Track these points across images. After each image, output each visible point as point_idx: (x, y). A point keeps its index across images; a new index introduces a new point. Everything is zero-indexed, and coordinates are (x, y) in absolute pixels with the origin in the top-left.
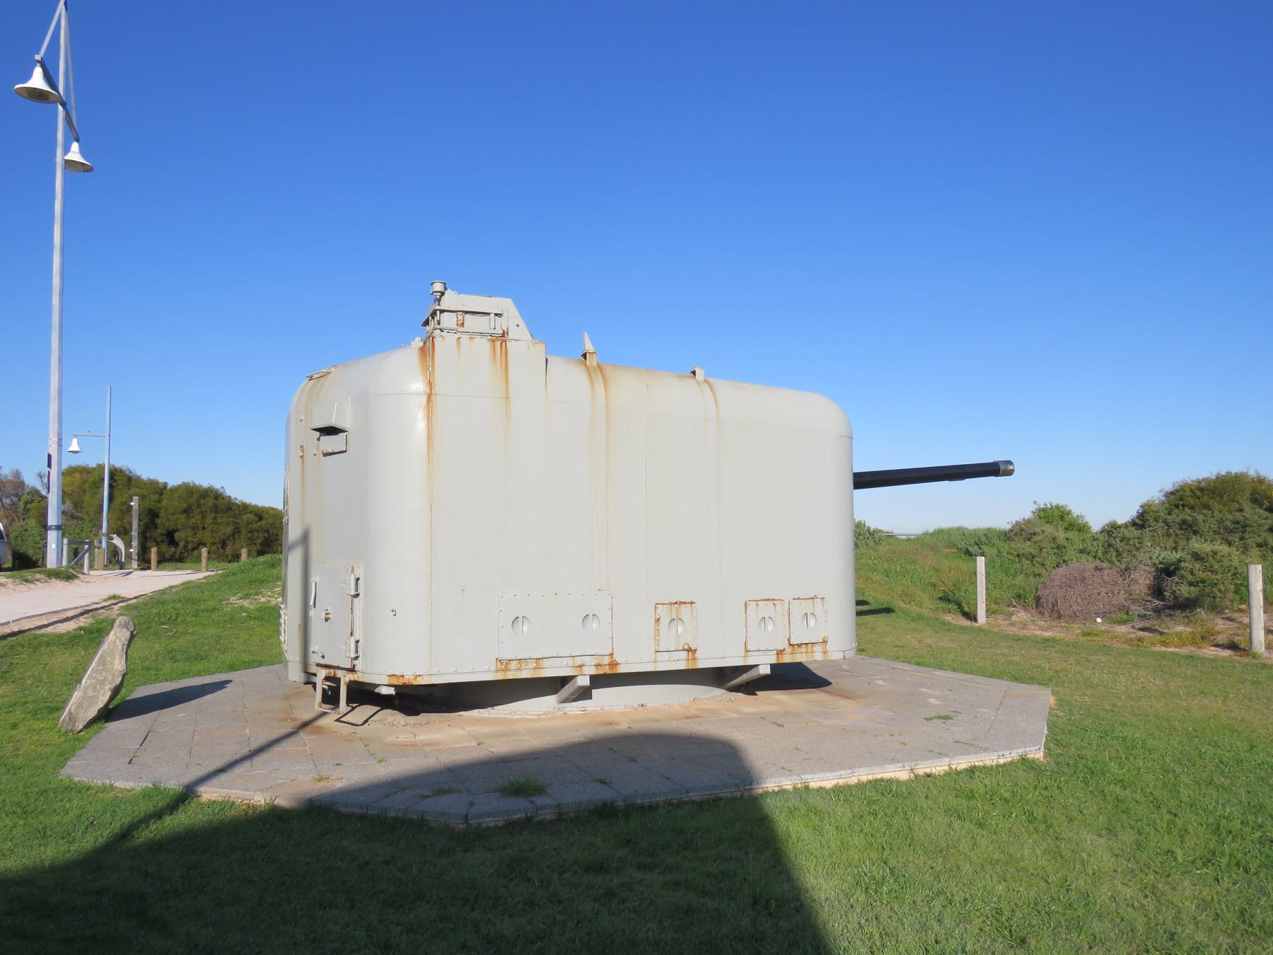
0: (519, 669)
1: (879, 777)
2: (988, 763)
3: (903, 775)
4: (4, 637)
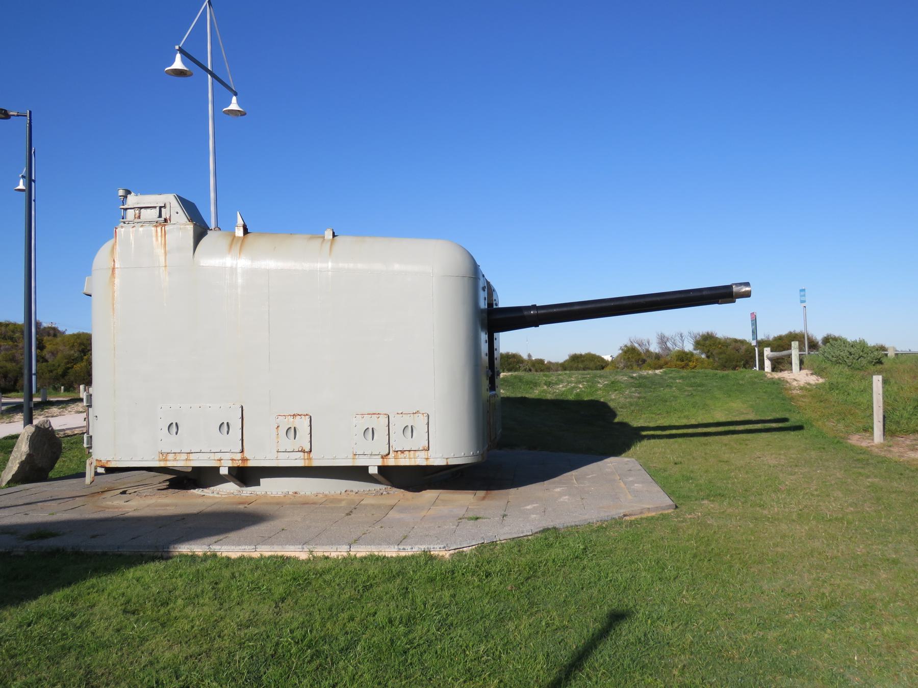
0: (175, 460)
1: (280, 554)
2: (388, 555)
3: (303, 556)
4: (915, 432)
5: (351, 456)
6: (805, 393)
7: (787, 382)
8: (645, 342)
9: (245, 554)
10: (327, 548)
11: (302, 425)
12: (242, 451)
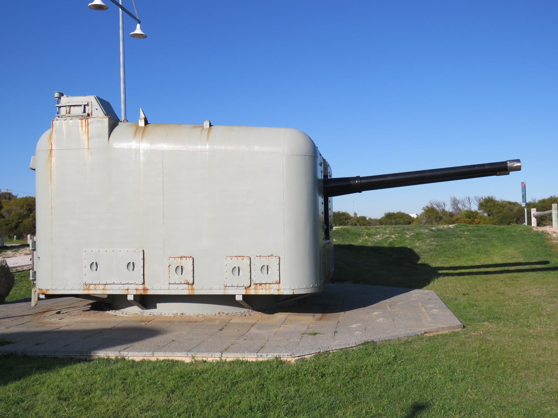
0: (95, 289)
1: (171, 358)
2: (250, 360)
3: (188, 360)
5: (223, 287)
7: (548, 234)
8: (442, 204)
10: (205, 354)
11: (187, 264)
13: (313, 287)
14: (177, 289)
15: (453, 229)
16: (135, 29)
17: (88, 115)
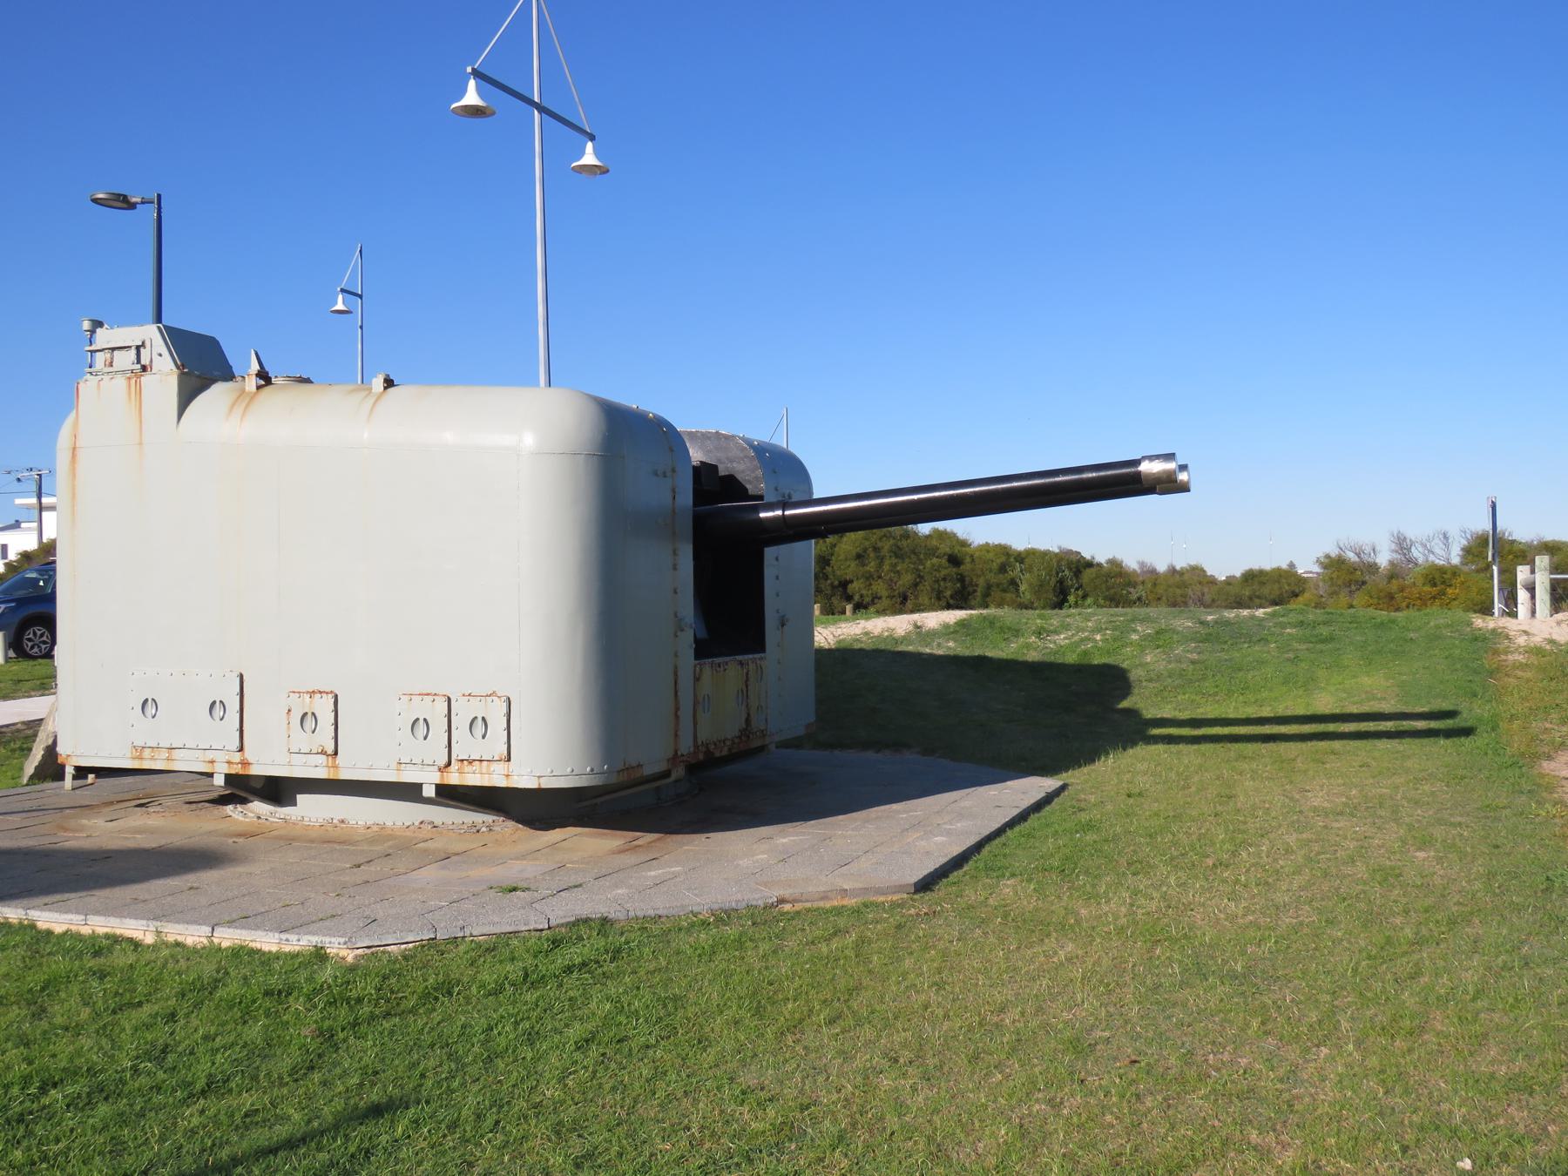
0: (152, 758)
5: (394, 766)
6: (1534, 660)
7: (1507, 637)
8: (1368, 550)
9: (74, 928)
10: (180, 928)
11: (324, 707)
12: (241, 749)
13: (609, 772)
14: (305, 765)
15: (1263, 619)
16: (582, 153)
17: (144, 368)
